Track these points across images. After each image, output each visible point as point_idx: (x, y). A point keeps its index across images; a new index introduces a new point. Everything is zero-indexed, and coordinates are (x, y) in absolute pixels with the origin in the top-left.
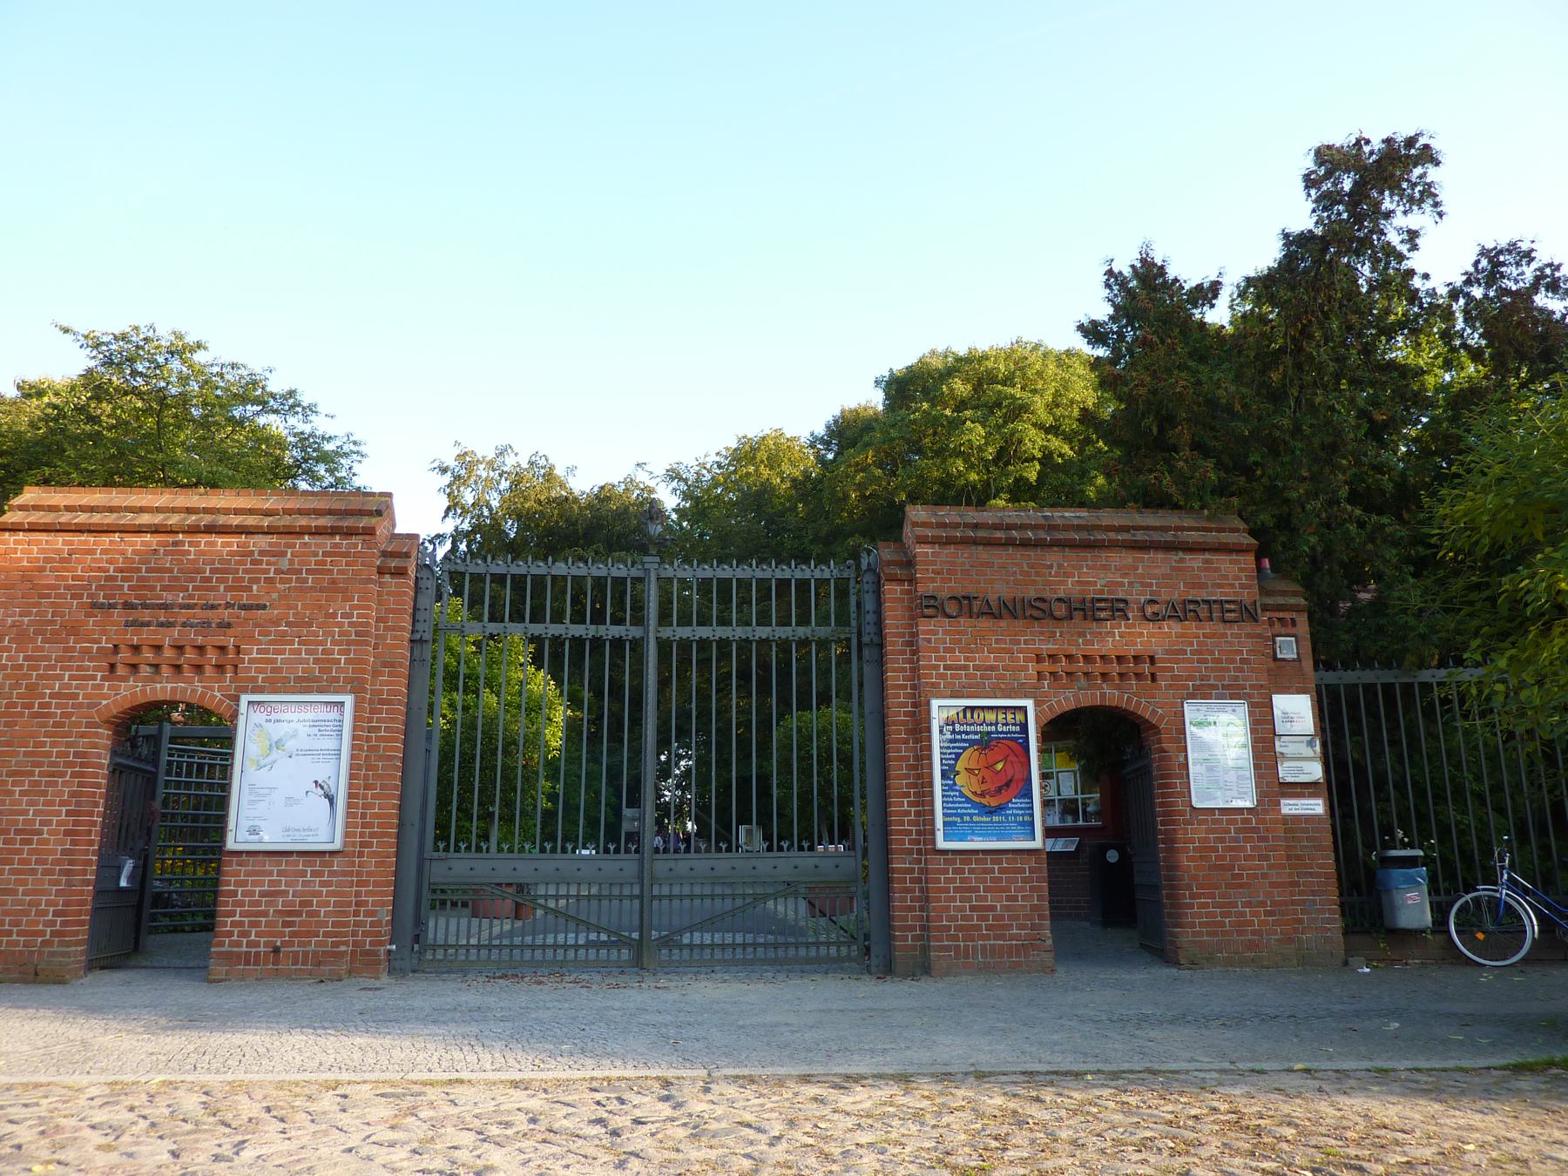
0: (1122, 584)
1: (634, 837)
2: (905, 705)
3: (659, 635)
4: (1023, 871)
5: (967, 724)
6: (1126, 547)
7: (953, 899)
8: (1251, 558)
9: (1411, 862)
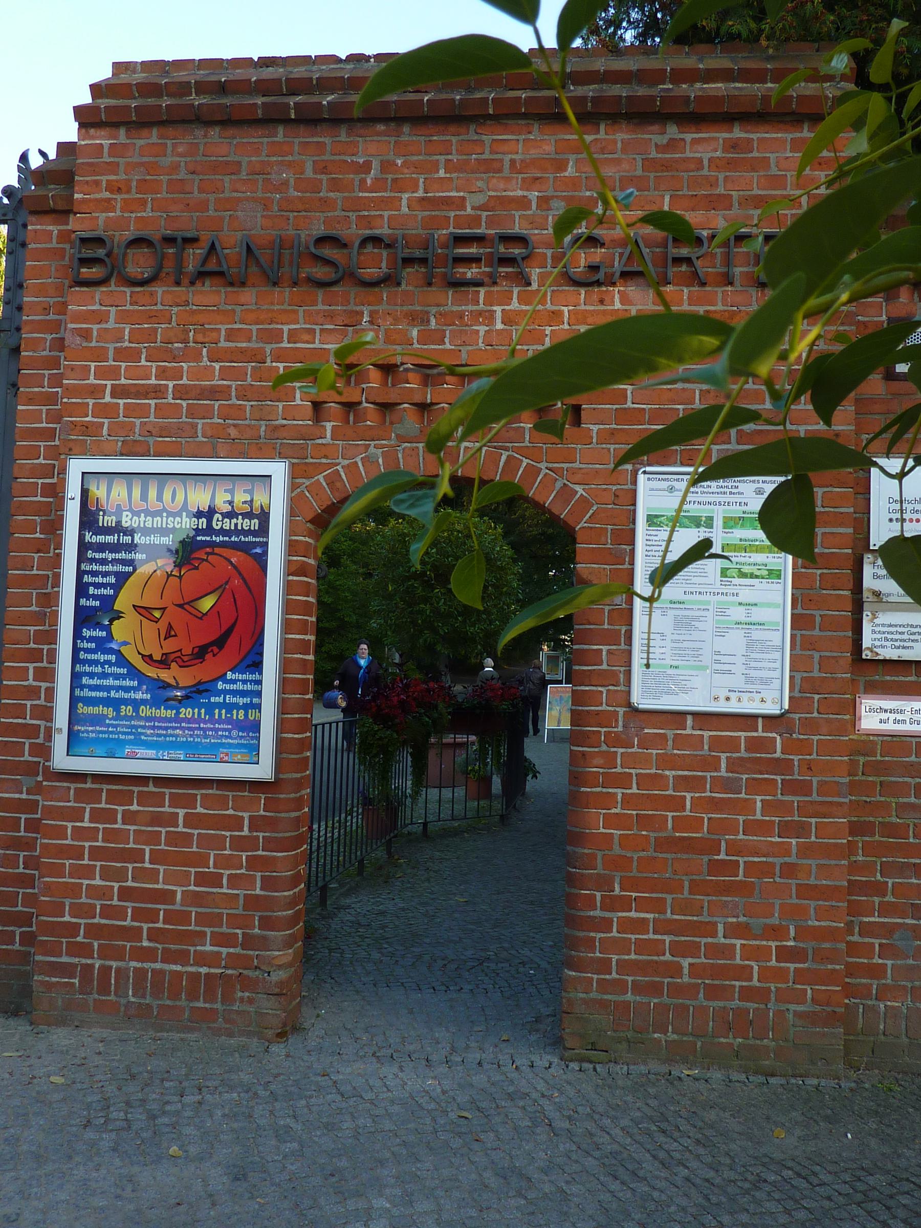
4: (235, 823)
5: (148, 513)
7: (88, 872)
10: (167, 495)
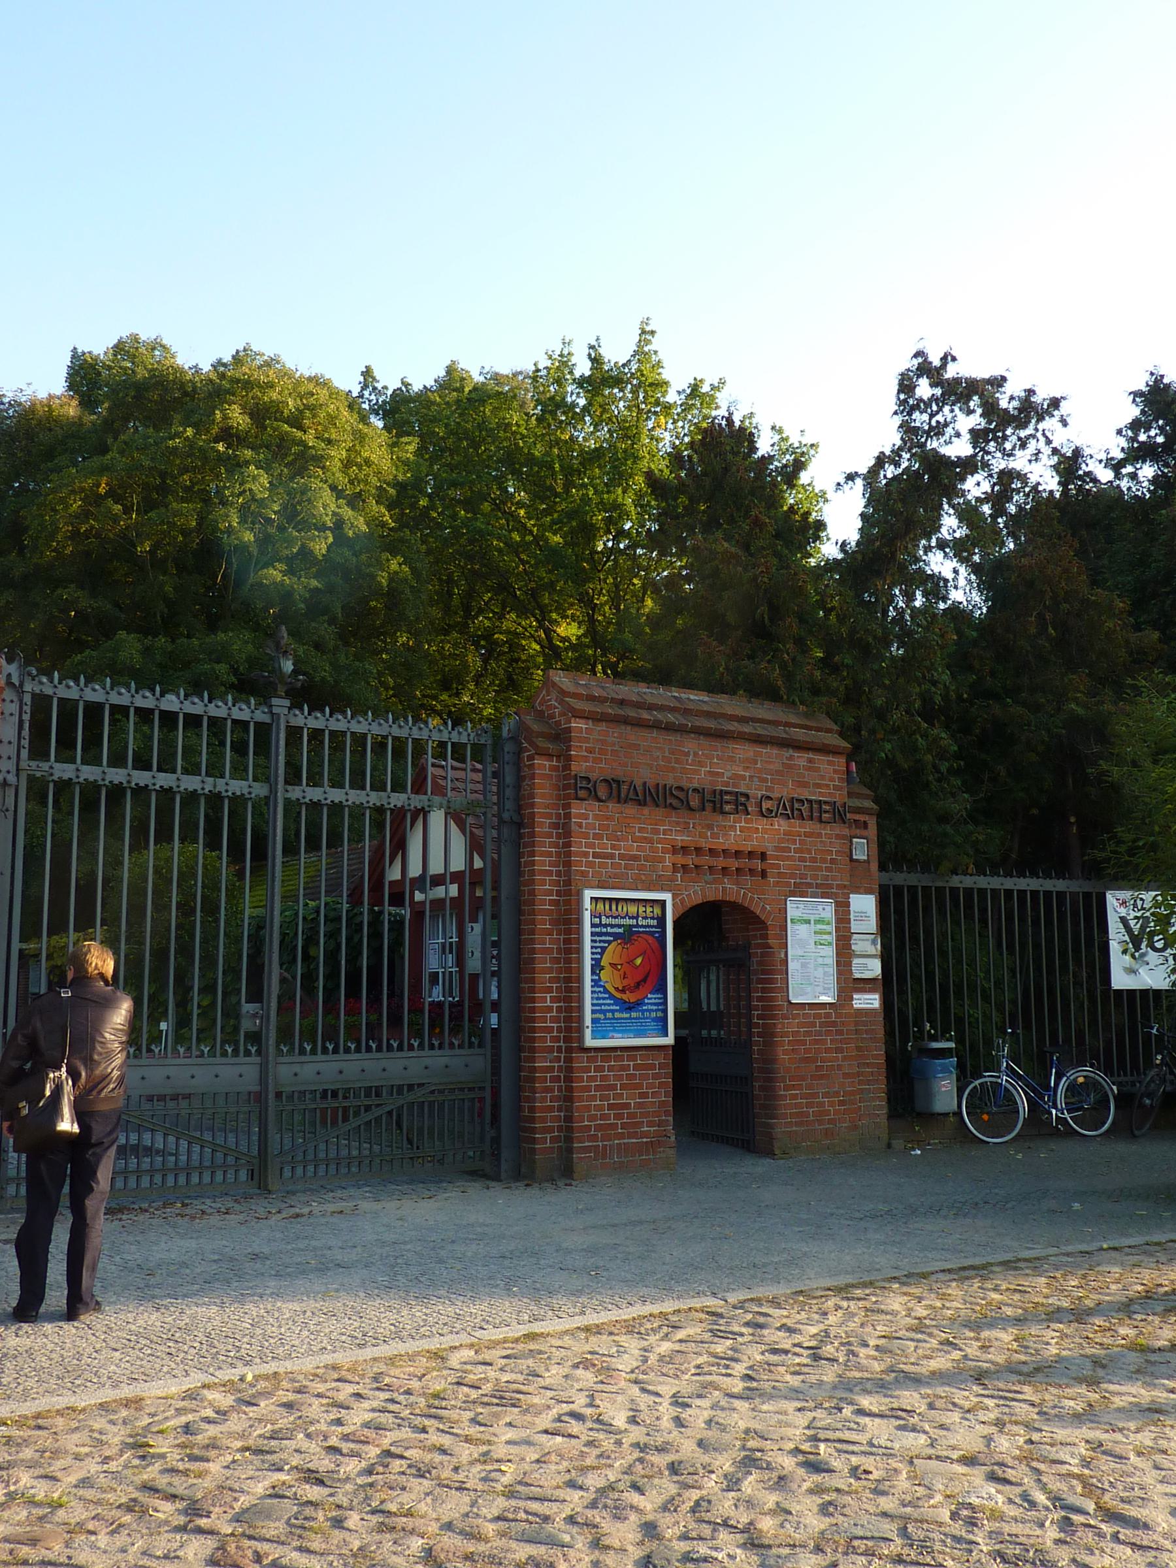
0: (743, 778)
1: (255, 1038)
2: (550, 893)
3: (288, 795)
4: (653, 1067)
5: (613, 917)
6: (777, 744)
7: (594, 1098)
8: (843, 760)
9: (943, 1053)
10: (620, 908)
